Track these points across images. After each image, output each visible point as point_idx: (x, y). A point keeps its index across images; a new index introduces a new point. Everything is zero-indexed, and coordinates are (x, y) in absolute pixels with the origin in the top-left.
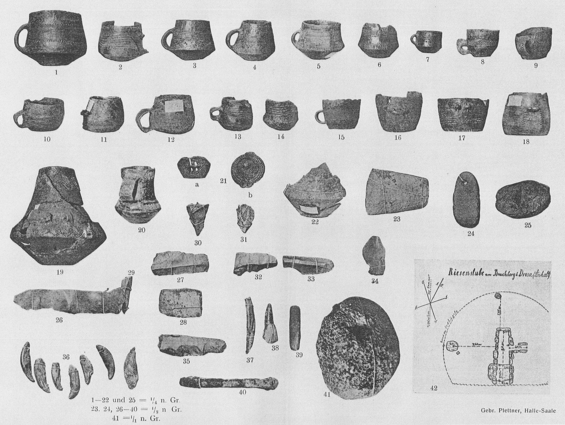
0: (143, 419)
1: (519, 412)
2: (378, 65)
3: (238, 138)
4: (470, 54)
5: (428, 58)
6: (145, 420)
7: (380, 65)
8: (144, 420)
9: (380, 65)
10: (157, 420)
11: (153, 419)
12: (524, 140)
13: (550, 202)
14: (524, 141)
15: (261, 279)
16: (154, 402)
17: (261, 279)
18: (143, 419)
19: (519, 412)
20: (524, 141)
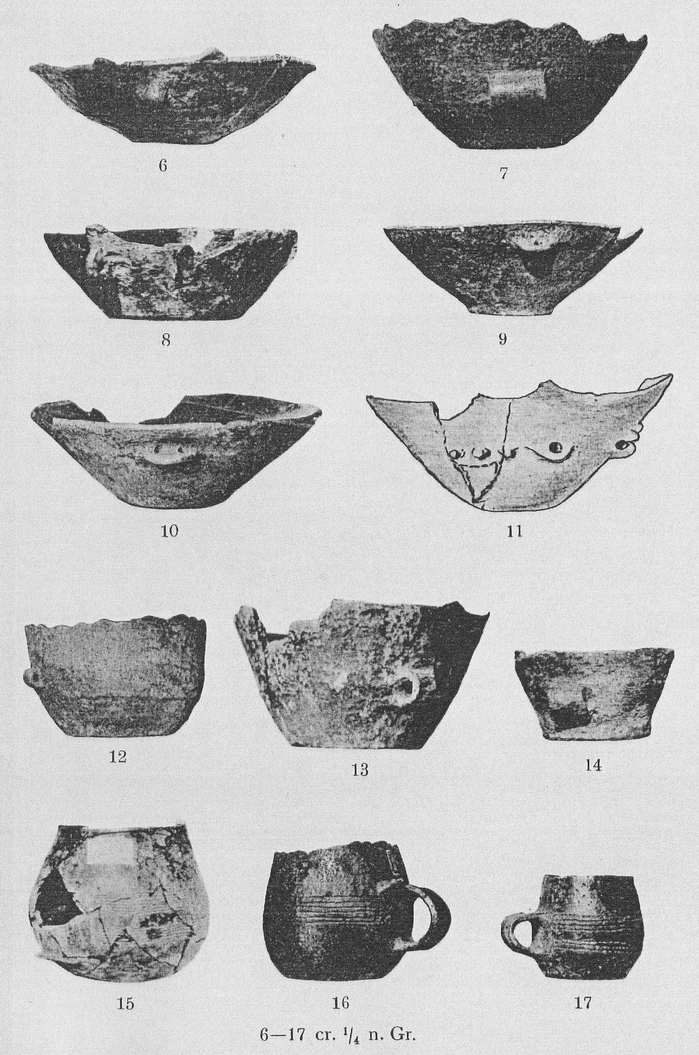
0: (374, 1035)
1: (327, 1039)
2: (505, 337)
3: (362, 773)
4: (610, 461)
5: (504, 171)
6: (379, 1038)
7: (503, 337)
8: (376, 1039)
9: (503, 337)
10: (408, 1039)
11: (397, 1036)
12: (520, 535)
13: (647, 43)
14: (519, 529)
15: (125, 761)
16: (353, 1039)
17: (125, 761)
18: (374, 1035)
19: (327, 1039)
20: (519, 529)
